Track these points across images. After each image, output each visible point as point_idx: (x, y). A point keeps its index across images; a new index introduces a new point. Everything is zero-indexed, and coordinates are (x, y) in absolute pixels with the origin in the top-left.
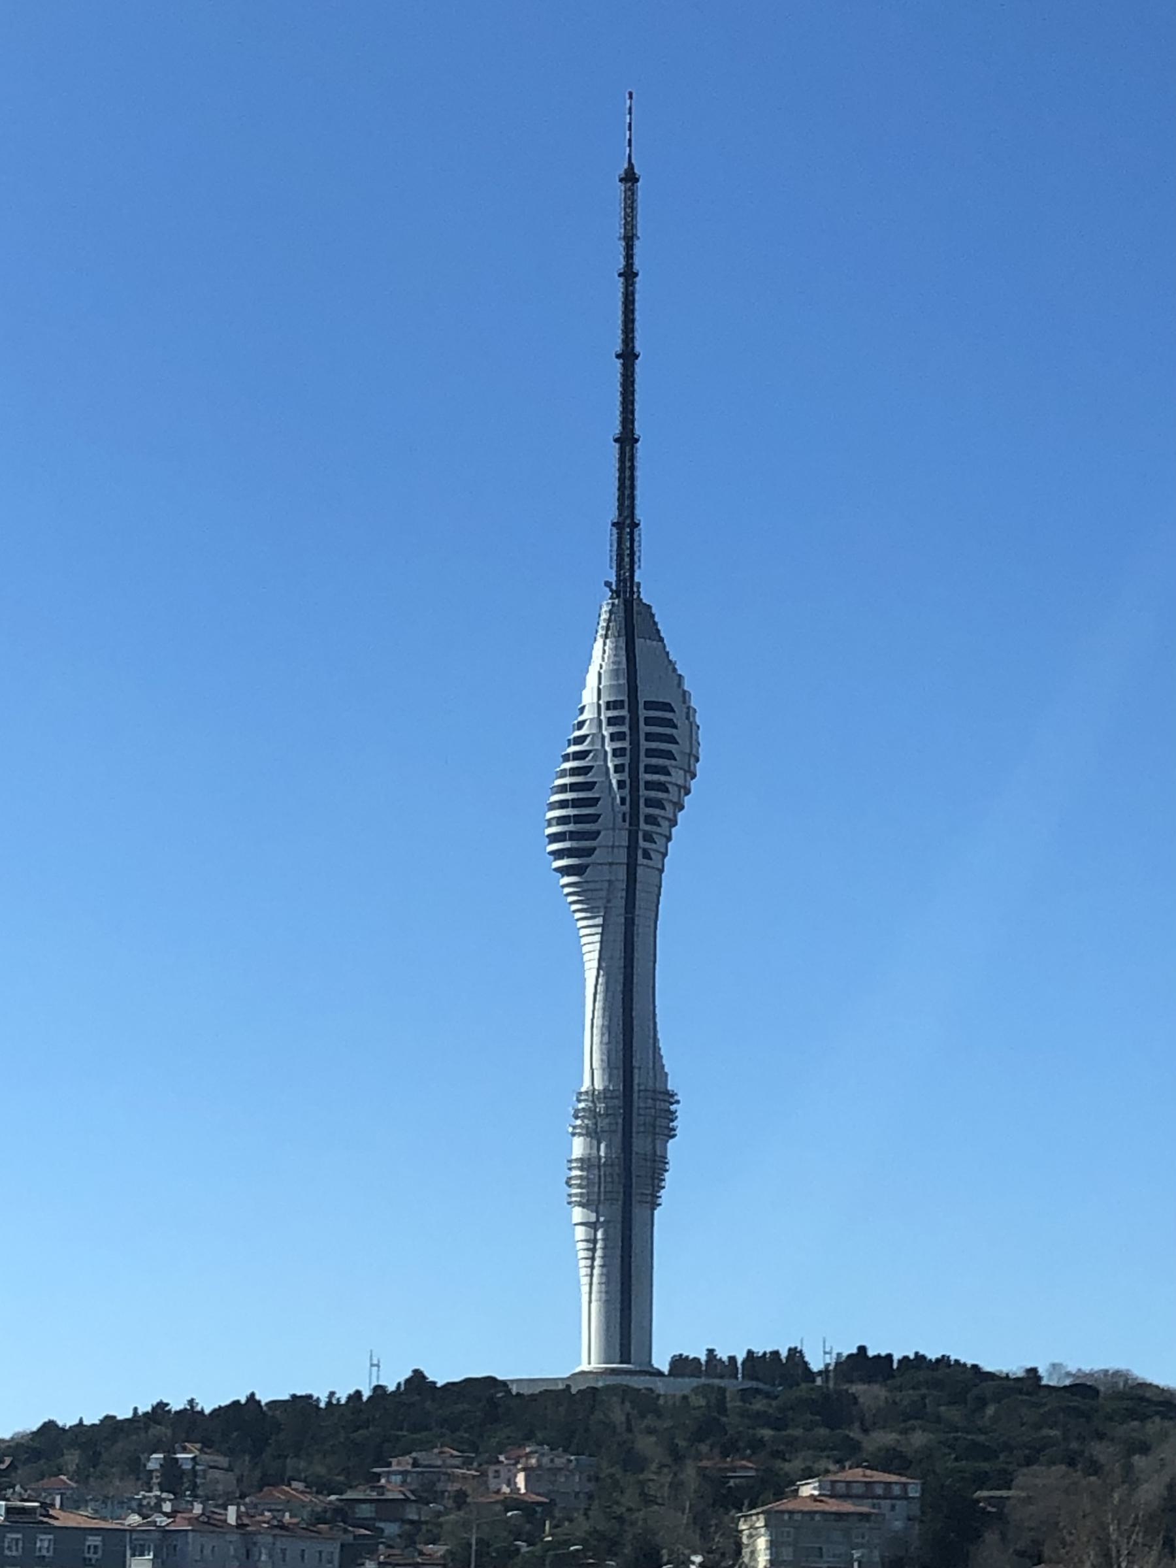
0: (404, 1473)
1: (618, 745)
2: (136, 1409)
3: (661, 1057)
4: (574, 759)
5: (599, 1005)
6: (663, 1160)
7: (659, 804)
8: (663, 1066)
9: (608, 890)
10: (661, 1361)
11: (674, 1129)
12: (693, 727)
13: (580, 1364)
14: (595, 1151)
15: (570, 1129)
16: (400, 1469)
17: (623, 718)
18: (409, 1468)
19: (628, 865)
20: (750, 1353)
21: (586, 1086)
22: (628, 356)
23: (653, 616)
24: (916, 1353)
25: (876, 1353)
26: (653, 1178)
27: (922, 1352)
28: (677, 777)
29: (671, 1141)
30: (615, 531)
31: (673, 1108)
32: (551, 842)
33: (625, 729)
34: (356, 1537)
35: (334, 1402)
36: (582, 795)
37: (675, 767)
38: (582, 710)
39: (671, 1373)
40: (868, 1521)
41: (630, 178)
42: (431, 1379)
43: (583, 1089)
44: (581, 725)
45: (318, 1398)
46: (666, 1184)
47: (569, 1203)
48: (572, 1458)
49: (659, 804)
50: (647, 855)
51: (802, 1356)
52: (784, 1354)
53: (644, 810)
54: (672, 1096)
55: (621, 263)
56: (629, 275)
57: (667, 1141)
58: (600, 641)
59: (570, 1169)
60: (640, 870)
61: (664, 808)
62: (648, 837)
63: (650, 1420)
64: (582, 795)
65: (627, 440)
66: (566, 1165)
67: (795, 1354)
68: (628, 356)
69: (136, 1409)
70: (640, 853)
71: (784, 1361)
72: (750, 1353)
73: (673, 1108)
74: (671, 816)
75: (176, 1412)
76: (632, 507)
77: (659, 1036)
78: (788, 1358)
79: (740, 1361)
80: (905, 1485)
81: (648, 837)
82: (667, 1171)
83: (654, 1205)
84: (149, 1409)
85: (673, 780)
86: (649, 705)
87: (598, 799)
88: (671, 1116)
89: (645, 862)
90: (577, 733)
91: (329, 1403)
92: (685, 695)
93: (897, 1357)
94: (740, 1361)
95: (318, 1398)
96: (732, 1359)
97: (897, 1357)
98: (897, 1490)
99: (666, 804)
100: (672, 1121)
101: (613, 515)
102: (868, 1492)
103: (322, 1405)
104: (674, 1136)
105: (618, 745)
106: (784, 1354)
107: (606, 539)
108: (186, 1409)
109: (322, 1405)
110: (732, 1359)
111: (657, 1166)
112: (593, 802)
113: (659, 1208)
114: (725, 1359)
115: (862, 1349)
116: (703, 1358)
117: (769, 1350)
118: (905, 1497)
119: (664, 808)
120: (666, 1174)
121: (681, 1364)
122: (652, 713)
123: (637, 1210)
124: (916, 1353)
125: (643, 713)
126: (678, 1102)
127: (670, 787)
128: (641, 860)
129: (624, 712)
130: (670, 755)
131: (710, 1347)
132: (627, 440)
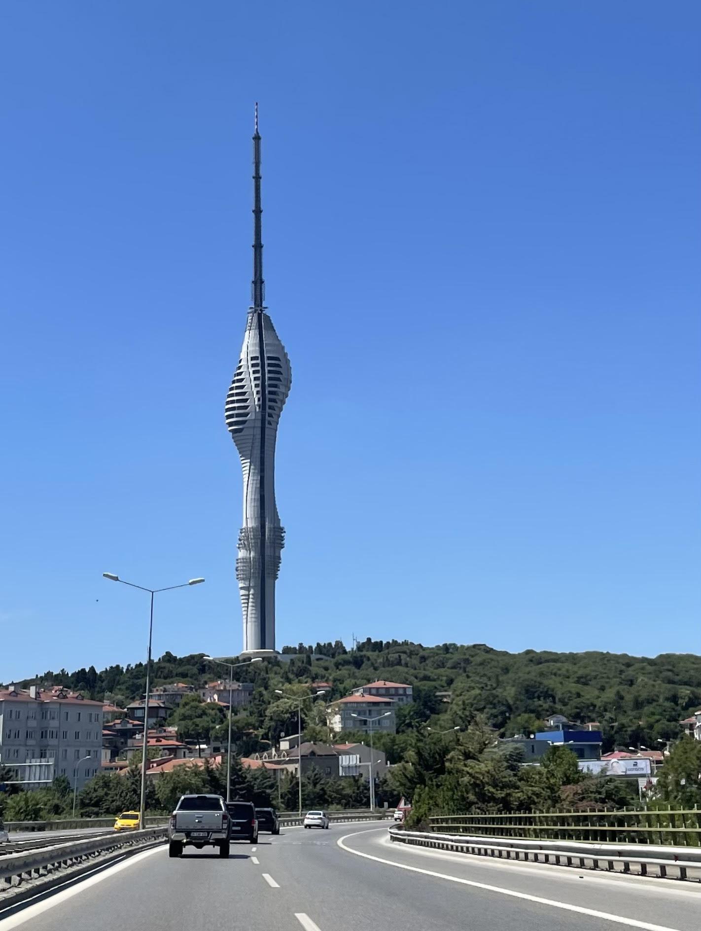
0: (160, 695)
1: (257, 382)
2: (37, 676)
3: (277, 513)
4: (236, 417)
5: (249, 489)
6: (279, 558)
7: (274, 401)
8: (278, 516)
9: (252, 446)
10: (279, 648)
11: (283, 545)
12: (289, 369)
13: (243, 650)
14: (248, 555)
15: (238, 545)
16: (158, 693)
17: (258, 364)
18: (162, 693)
19: (262, 427)
20: (318, 644)
21: (244, 525)
22: (258, 212)
23: (270, 320)
24: (393, 640)
25: (375, 641)
26: (274, 566)
27: (395, 639)
28: (282, 389)
29: (282, 550)
30: (253, 285)
31: (283, 535)
32: (230, 426)
33: (259, 368)
34: (134, 725)
35: (130, 668)
36: (242, 404)
37: (282, 385)
38: (240, 361)
39: (283, 653)
40: (390, 705)
41: (257, 138)
42: (174, 655)
43: (244, 527)
44: (240, 368)
45: (122, 668)
46: (281, 568)
47: (237, 578)
48: (241, 684)
49: (274, 401)
50: (270, 423)
51: (342, 645)
52: (333, 644)
53: (268, 403)
54: (282, 529)
55: (253, 173)
56: (257, 178)
57: (280, 550)
58: (248, 332)
59: (237, 563)
60: (267, 430)
61: (277, 403)
62: (270, 415)
63: (276, 668)
64: (242, 404)
65: (258, 247)
66: (235, 562)
67: (339, 644)
68: (258, 212)
69: (37, 676)
70: (267, 422)
71: (333, 646)
72: (318, 644)
73: (283, 535)
74: (280, 406)
75: (55, 675)
76: (261, 275)
77: (277, 503)
78: (335, 646)
79: (314, 648)
80: (405, 689)
81: (270, 415)
82: (280, 563)
83: (275, 577)
84: (43, 675)
85: (281, 390)
86: (269, 358)
87: (248, 406)
88: (282, 539)
89: (269, 426)
90: (238, 371)
91: (127, 669)
92: (285, 355)
93: (384, 642)
94: (314, 648)
95: (122, 668)
96: (311, 647)
97: (384, 642)
98: (401, 692)
99: (276, 409)
100: (283, 541)
101: (252, 278)
102: (387, 692)
103: (124, 670)
104: (283, 548)
105: (257, 382)
106: (333, 644)
107: (249, 288)
108: (59, 674)
109: (124, 670)
110: (311, 647)
111: (276, 560)
112: (245, 400)
113: (277, 580)
114: (307, 647)
115: (369, 640)
116: (297, 648)
117: (326, 642)
118: (405, 694)
119: (277, 403)
120: (280, 565)
121: (287, 650)
122: (270, 362)
123: (268, 581)
124: (393, 640)
125: (266, 362)
126: (285, 532)
127: (278, 401)
128: (267, 425)
129: (259, 368)
130: (279, 379)
131: (301, 642)
132: (258, 247)
